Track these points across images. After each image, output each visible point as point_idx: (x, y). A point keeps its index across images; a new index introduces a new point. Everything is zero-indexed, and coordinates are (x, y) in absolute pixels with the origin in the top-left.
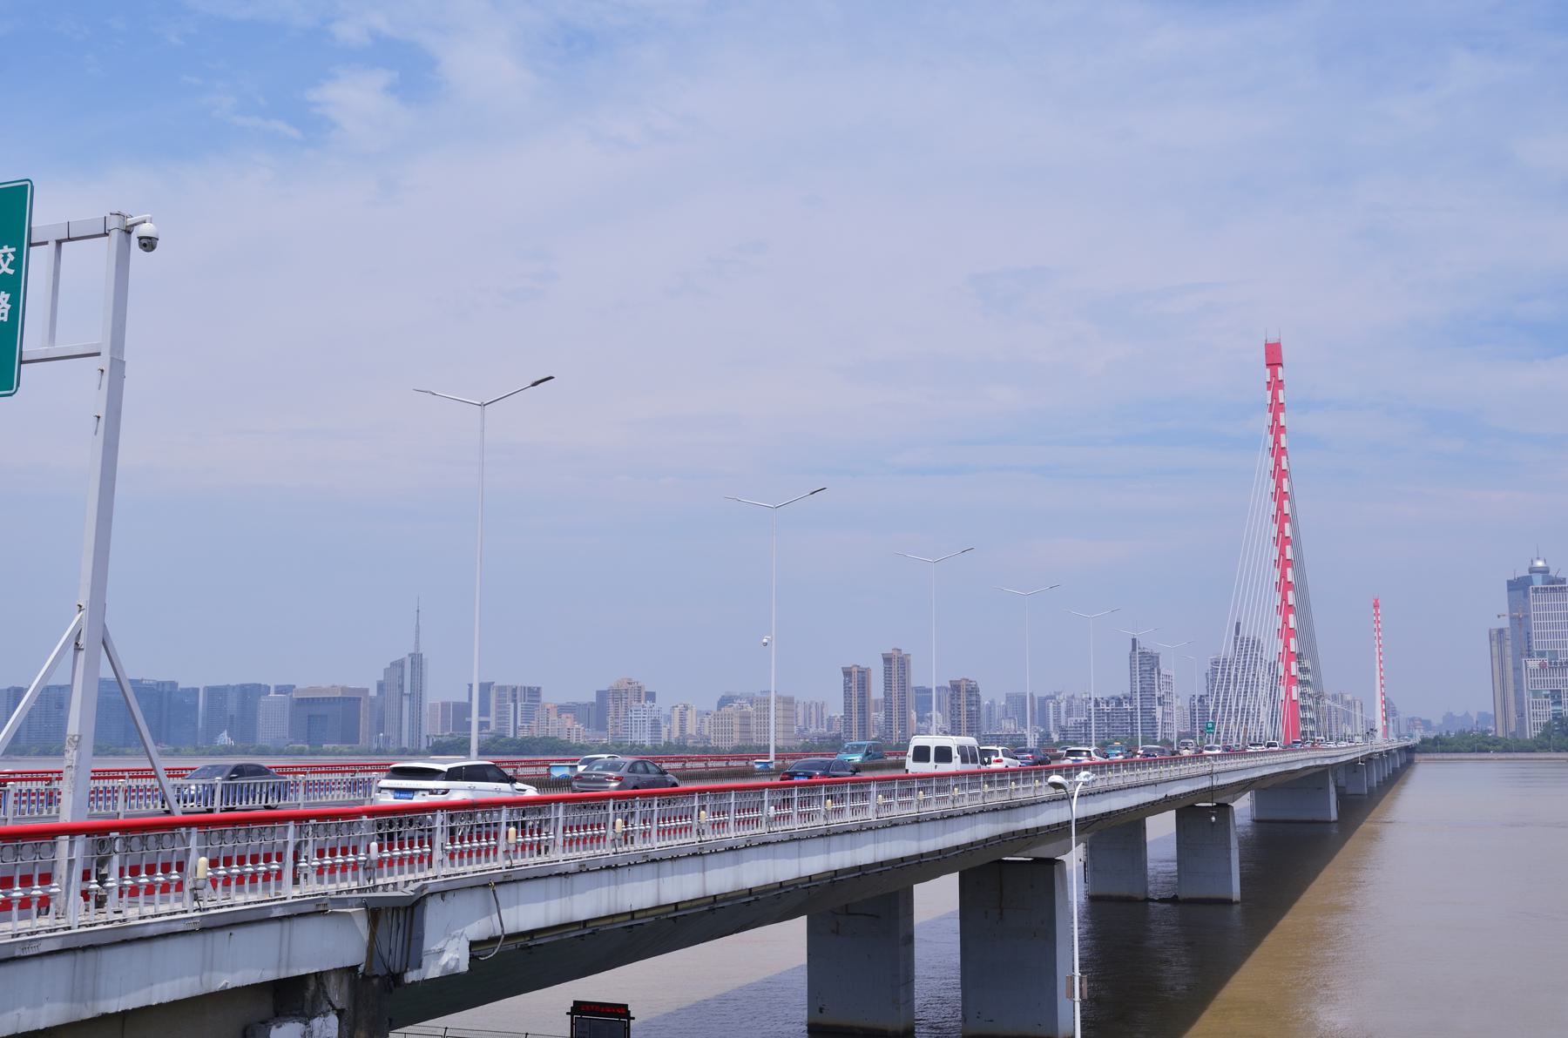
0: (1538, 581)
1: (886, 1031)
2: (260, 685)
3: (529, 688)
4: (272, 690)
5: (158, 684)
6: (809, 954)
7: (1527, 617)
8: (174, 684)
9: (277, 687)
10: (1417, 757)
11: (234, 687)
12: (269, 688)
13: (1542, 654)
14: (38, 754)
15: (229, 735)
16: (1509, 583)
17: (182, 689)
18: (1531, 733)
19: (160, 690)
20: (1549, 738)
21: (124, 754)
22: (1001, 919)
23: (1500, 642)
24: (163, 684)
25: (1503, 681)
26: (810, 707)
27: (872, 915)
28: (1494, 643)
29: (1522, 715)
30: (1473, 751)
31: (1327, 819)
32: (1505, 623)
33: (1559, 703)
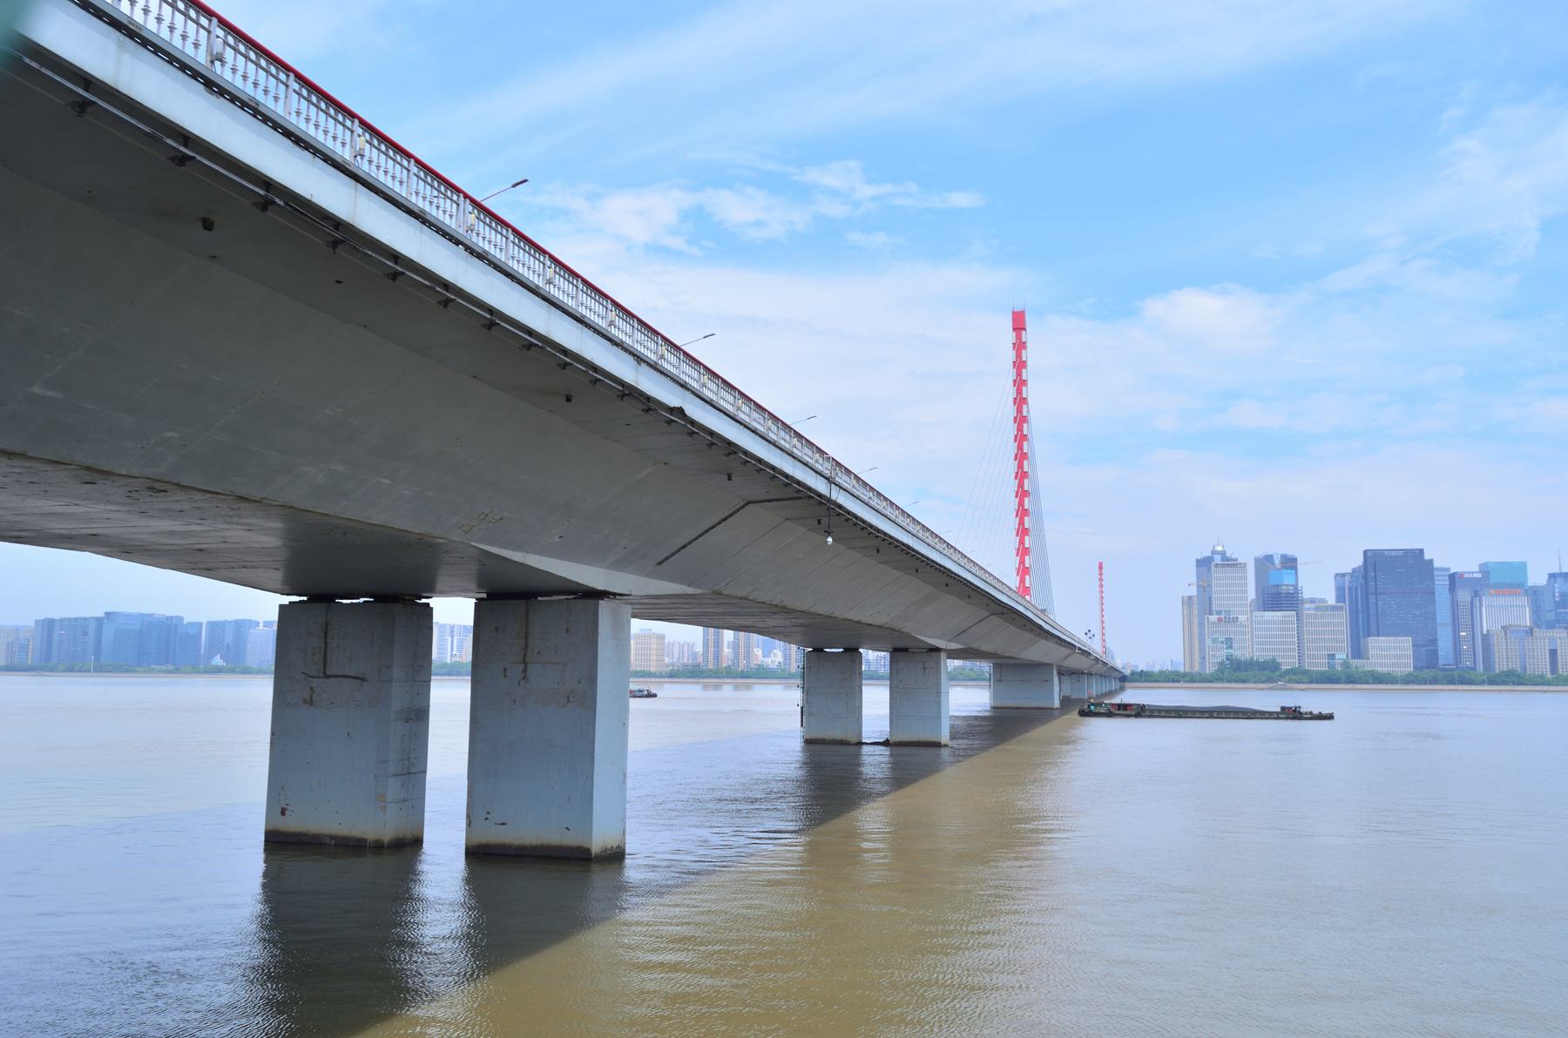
0: (1218, 559)
1: (365, 840)
2: (251, 621)
3: (464, 626)
4: (261, 625)
5: (167, 618)
6: (273, 734)
7: (1210, 586)
8: (181, 619)
9: (265, 622)
10: (1127, 685)
11: (230, 622)
12: (258, 623)
13: (1219, 613)
14: (65, 671)
15: (221, 658)
16: (1198, 561)
17: (189, 623)
18: (1210, 669)
19: (169, 622)
20: (1223, 674)
21: (135, 672)
22: (524, 678)
23: (1190, 606)
24: (172, 618)
25: (1191, 634)
26: (683, 646)
27: (356, 678)
28: (1185, 606)
29: (1204, 658)
30: (1168, 681)
31: (1051, 706)
32: (1193, 591)
33: (1231, 647)
